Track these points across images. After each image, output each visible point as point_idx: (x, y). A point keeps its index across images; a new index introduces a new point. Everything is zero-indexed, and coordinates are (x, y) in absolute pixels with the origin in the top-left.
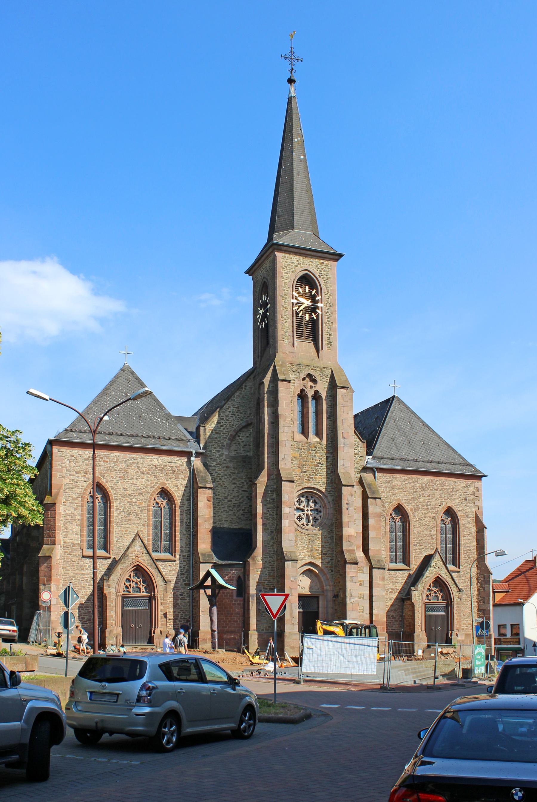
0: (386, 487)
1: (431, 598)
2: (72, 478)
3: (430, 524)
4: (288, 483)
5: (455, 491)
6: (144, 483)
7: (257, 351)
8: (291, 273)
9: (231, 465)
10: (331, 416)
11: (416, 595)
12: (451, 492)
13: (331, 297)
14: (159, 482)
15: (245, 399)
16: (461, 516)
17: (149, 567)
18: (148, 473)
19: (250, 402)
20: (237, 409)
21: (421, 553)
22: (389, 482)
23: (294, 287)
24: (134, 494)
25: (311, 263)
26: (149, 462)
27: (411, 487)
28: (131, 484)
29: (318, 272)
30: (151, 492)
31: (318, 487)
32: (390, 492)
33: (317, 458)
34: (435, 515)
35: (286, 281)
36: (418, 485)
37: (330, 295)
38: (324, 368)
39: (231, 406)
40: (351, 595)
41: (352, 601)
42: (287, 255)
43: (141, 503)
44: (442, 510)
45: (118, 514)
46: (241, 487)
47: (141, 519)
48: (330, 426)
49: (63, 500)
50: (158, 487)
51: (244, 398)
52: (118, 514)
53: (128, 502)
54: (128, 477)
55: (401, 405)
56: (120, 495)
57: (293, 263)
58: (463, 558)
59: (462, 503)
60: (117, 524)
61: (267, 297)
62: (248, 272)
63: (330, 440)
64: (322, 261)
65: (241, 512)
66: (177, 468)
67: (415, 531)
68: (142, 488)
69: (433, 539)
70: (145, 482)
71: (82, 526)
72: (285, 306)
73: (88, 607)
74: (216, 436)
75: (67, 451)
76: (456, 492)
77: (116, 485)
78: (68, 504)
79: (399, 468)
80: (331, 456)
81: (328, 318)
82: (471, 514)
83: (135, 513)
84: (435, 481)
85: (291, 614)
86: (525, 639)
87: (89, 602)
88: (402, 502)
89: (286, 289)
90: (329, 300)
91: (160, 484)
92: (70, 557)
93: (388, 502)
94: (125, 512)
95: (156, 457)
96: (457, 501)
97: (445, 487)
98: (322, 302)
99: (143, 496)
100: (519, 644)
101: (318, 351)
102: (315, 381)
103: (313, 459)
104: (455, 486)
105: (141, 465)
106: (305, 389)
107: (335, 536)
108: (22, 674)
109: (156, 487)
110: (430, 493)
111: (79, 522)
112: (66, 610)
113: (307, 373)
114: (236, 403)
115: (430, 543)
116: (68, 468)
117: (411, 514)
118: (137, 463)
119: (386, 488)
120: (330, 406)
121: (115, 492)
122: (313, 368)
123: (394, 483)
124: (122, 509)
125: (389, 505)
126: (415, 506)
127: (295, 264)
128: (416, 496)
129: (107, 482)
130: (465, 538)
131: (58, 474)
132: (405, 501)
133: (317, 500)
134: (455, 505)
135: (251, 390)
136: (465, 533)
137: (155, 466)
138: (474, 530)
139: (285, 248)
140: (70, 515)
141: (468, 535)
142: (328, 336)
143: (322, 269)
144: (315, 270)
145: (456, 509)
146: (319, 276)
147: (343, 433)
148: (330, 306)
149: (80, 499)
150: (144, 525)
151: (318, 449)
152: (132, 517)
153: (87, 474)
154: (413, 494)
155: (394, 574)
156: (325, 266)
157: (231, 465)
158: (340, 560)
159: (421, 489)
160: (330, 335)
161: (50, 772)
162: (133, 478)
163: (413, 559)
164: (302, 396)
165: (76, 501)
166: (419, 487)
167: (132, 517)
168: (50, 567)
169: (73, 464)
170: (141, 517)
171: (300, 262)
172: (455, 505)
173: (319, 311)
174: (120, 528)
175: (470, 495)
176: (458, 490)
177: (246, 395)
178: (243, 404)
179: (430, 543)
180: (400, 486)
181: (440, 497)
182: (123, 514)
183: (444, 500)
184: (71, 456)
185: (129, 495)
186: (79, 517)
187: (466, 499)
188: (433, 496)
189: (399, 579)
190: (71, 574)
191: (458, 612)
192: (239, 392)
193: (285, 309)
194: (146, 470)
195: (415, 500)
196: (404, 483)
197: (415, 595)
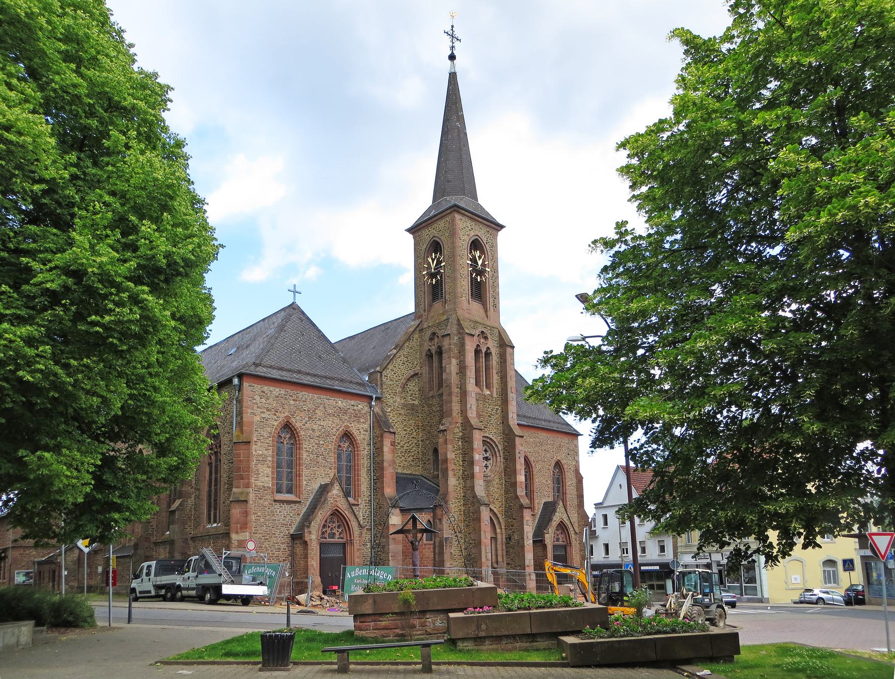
1: (326, 535)
2: (263, 415)
4: (477, 431)
7: (422, 306)
9: (402, 412)
17: (346, 512)
18: (334, 415)
31: (491, 436)
36: (538, 440)
43: (328, 446)
49: (255, 439)
61: (441, 254)
65: (411, 458)
66: (359, 411)
71: (273, 468)
74: (391, 383)
75: (258, 387)
78: (259, 444)
85: (486, 556)
92: (261, 501)
101: (486, 311)
102: (486, 338)
108: (6, 641)
111: (270, 464)
116: (260, 405)
128: (536, 449)
131: (249, 411)
133: (488, 449)
138: (574, 481)
139: (463, 212)
140: (261, 455)
145: (563, 462)
149: (271, 439)
150: (331, 469)
152: (320, 459)
157: (402, 412)
164: (477, 352)
165: (267, 441)
167: (320, 459)
168: (246, 513)
169: (263, 400)
184: (262, 392)
186: (270, 459)
190: (262, 520)
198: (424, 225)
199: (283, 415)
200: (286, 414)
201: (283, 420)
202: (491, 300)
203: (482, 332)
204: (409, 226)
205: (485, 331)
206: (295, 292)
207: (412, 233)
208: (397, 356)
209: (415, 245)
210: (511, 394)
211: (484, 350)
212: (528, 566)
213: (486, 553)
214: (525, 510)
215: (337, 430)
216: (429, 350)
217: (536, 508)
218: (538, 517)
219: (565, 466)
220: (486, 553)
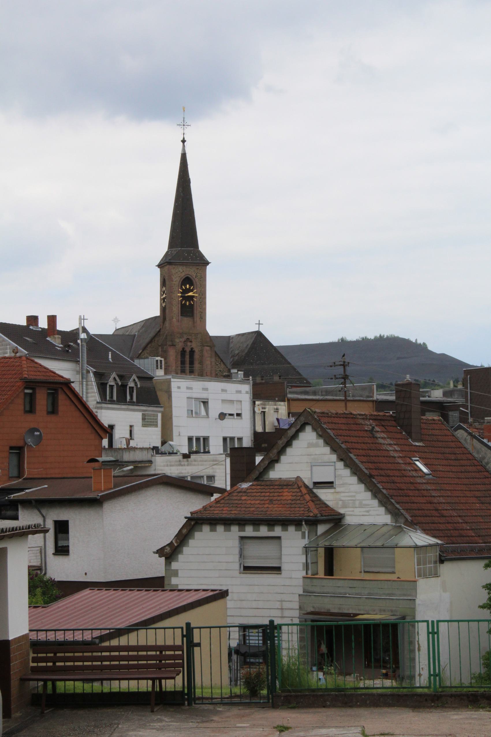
23: (180, 285)
29: (195, 275)
38: (197, 334)
57: (179, 271)
64: (197, 267)
81: (201, 303)
86: (288, 528)
112: (227, 415)
146: (196, 277)
148: (202, 295)
164: (183, 352)
173: (195, 299)
204: (157, 265)
206: (259, 324)
211: (188, 350)
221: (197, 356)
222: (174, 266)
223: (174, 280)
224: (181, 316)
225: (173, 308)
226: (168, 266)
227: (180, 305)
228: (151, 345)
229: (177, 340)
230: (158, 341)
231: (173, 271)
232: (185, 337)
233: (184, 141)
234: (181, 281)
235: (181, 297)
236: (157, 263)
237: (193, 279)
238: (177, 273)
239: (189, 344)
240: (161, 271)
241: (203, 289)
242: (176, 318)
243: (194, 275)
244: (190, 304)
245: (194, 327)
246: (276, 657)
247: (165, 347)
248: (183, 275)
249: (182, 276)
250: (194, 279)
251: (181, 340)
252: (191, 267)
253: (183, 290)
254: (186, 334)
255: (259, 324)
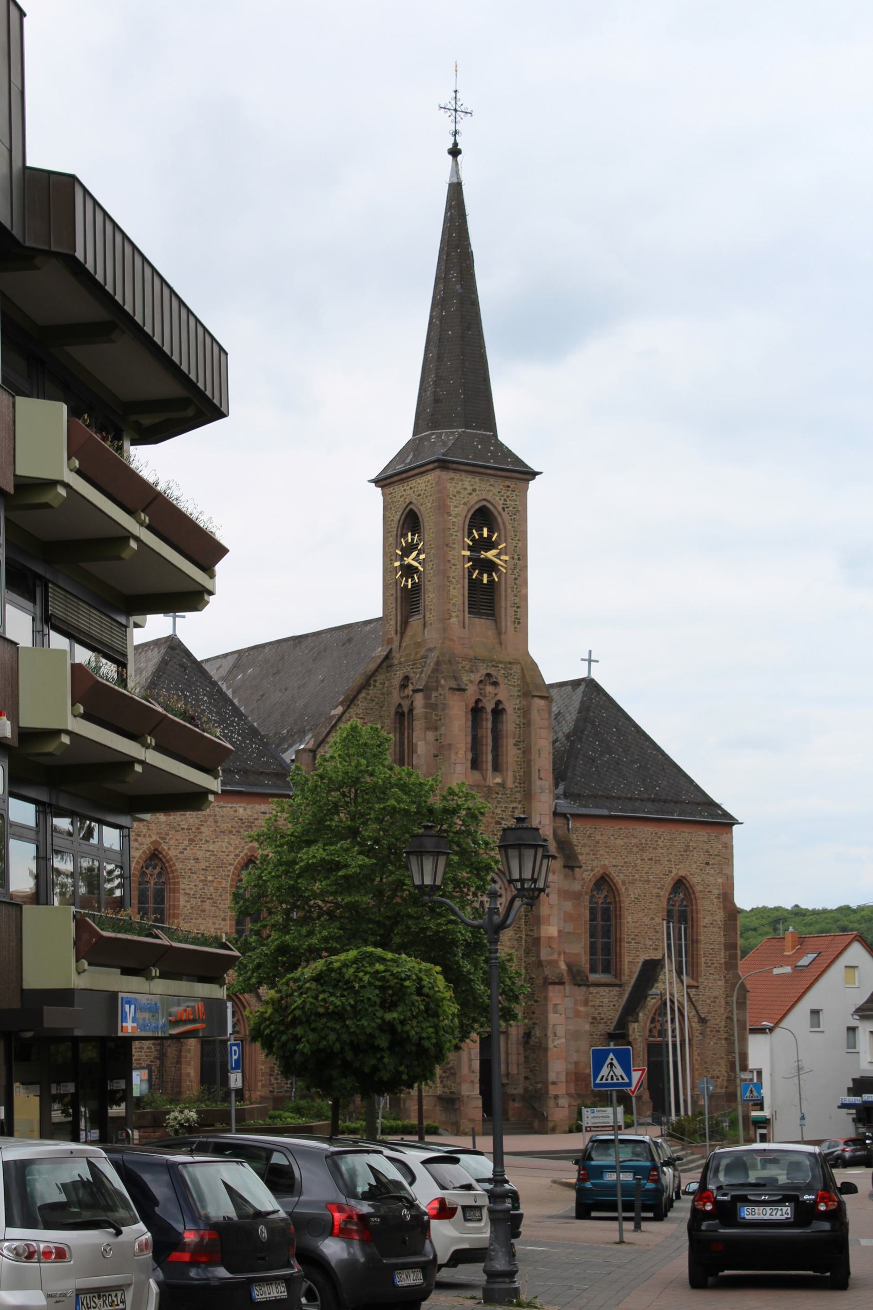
0: (584, 845)
3: (653, 906)
5: (691, 849)
6: (224, 849)
8: (462, 506)
10: (520, 742)
11: (636, 1030)
12: (685, 851)
13: (520, 543)
14: (247, 847)
15: (374, 703)
16: (701, 891)
18: (231, 832)
19: (382, 707)
20: (362, 721)
21: (638, 956)
22: (590, 837)
23: (466, 527)
24: (209, 867)
25: (492, 488)
26: (232, 813)
27: (623, 844)
28: (206, 850)
30: (236, 863)
32: (592, 853)
33: (498, 811)
34: (659, 891)
35: (454, 520)
36: (634, 841)
37: (519, 540)
38: (510, 663)
39: (354, 716)
40: (555, 1034)
41: (556, 1043)
42: (457, 476)
43: (220, 883)
44: (669, 882)
45: (187, 902)
46: (447, 800)
47: (220, 909)
48: (518, 757)
50: (246, 854)
51: (373, 701)
52: (187, 902)
53: (201, 881)
54: (201, 840)
55: (601, 696)
56: (190, 869)
57: (465, 489)
58: (703, 964)
59: (701, 870)
60: (184, 919)
62: (377, 482)
63: (518, 781)
64: (508, 483)
67: (630, 920)
68: (222, 857)
69: (657, 932)
70: (227, 848)
72: (453, 562)
73: (140, 1060)
76: (692, 851)
77: (182, 853)
79: (605, 812)
80: (520, 806)
81: (516, 579)
82: (717, 889)
83: (212, 899)
84: (660, 833)
85: (470, 1066)
87: (141, 1052)
88: (610, 869)
89: (455, 534)
90: (517, 549)
91: (248, 849)
93: (587, 871)
94: (196, 898)
95: (242, 805)
96: (694, 866)
97: (675, 843)
98: (506, 554)
99: (224, 871)
100: (762, 1109)
101: (499, 633)
103: (493, 813)
104: (691, 840)
105: (219, 819)
106: (481, 698)
107: (524, 936)
109: (242, 855)
110: (652, 855)
113: (485, 672)
114: (361, 711)
115: (652, 939)
117: (623, 890)
118: (215, 816)
119: (585, 846)
120: (519, 725)
121: (181, 866)
122: (494, 663)
123: (598, 837)
124: (192, 893)
125: (589, 875)
126: (628, 876)
127: (468, 491)
129: (169, 849)
130: (706, 930)
132: (613, 868)
134: (691, 874)
135: (383, 688)
136: (706, 921)
137: (241, 820)
139: (454, 466)
141: (711, 924)
142: (515, 609)
143: (508, 497)
144: (497, 499)
145: (695, 880)
146: (503, 509)
147: (539, 770)
148: (519, 559)
150: (224, 920)
151: (500, 796)
152: (207, 905)
153: (139, 836)
154: (627, 856)
155: (596, 993)
156: (512, 491)
158: (534, 976)
159: (638, 847)
160: (518, 607)
161: (522, 1225)
162: (207, 841)
163: (626, 966)
164: (476, 711)
166: (635, 844)
167: (207, 905)
170: (220, 906)
171: (474, 487)
172: (691, 874)
174: (189, 924)
175: (716, 855)
176: (695, 848)
177: (375, 697)
178: (371, 712)
179: (652, 939)
180: (606, 843)
181: (668, 861)
182: (193, 901)
183: (673, 866)
185: (203, 869)
187: (707, 864)
188: (657, 858)
189: (604, 1000)
191: (699, 1058)
192: (366, 691)
193: (454, 567)
194: (227, 827)
195: (629, 867)
196: (612, 838)
197: (634, 1029)
198: (396, 478)
199: (148, 841)
200: (154, 838)
201: (149, 848)
202: (511, 611)
203: (489, 675)
204: (373, 477)
205: (494, 673)
206: (590, 661)
207: (382, 487)
208: (344, 718)
209: (385, 509)
210: (539, 783)
211: (489, 706)
212: (554, 1083)
213: (470, 1060)
214: (551, 988)
215: (237, 855)
216: (400, 705)
217: (626, 972)
218: (628, 989)
219: (698, 888)
220: (470, 1060)
221: (510, 722)
222: (452, 474)
223: (453, 513)
224: (470, 613)
225: (451, 588)
226: (438, 472)
227: (466, 581)
228: (368, 694)
229: (465, 678)
230: (383, 684)
231: (451, 488)
232: (483, 671)
233: (455, 152)
234: (469, 516)
235: (470, 559)
236: (376, 471)
237: (496, 514)
238: (459, 492)
239: (489, 689)
240: (383, 494)
241: (520, 544)
242: (457, 616)
243: (500, 504)
244: (491, 581)
245: (501, 643)
246: (28, 1189)
247: (434, 694)
248: (474, 501)
249: (472, 503)
250: (500, 514)
251: (472, 676)
252: (492, 481)
253: (473, 540)
254: (483, 661)
255: (590, 661)
